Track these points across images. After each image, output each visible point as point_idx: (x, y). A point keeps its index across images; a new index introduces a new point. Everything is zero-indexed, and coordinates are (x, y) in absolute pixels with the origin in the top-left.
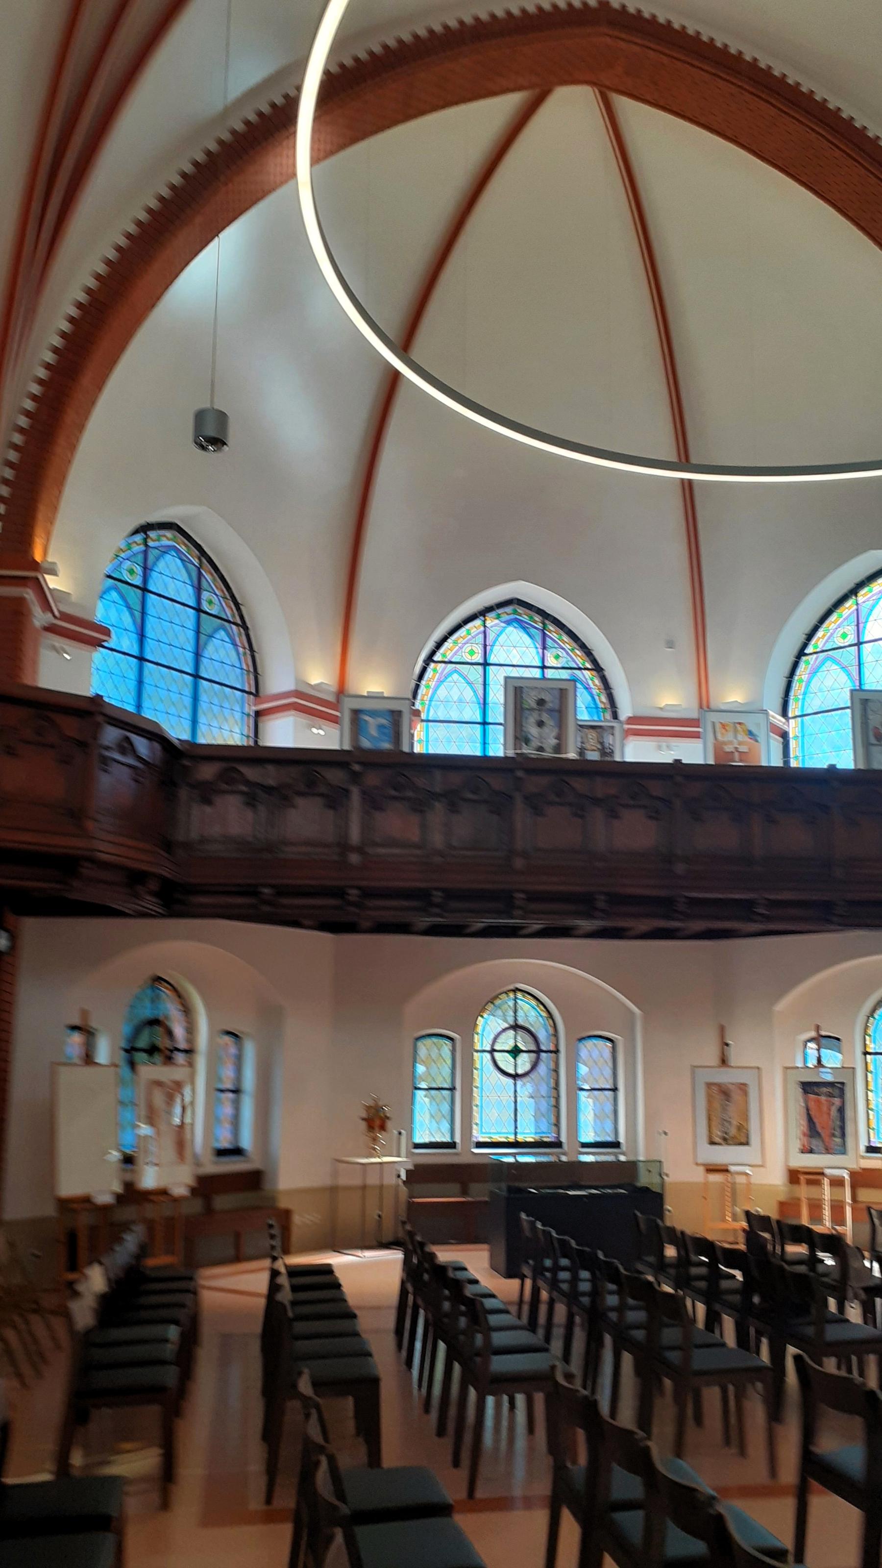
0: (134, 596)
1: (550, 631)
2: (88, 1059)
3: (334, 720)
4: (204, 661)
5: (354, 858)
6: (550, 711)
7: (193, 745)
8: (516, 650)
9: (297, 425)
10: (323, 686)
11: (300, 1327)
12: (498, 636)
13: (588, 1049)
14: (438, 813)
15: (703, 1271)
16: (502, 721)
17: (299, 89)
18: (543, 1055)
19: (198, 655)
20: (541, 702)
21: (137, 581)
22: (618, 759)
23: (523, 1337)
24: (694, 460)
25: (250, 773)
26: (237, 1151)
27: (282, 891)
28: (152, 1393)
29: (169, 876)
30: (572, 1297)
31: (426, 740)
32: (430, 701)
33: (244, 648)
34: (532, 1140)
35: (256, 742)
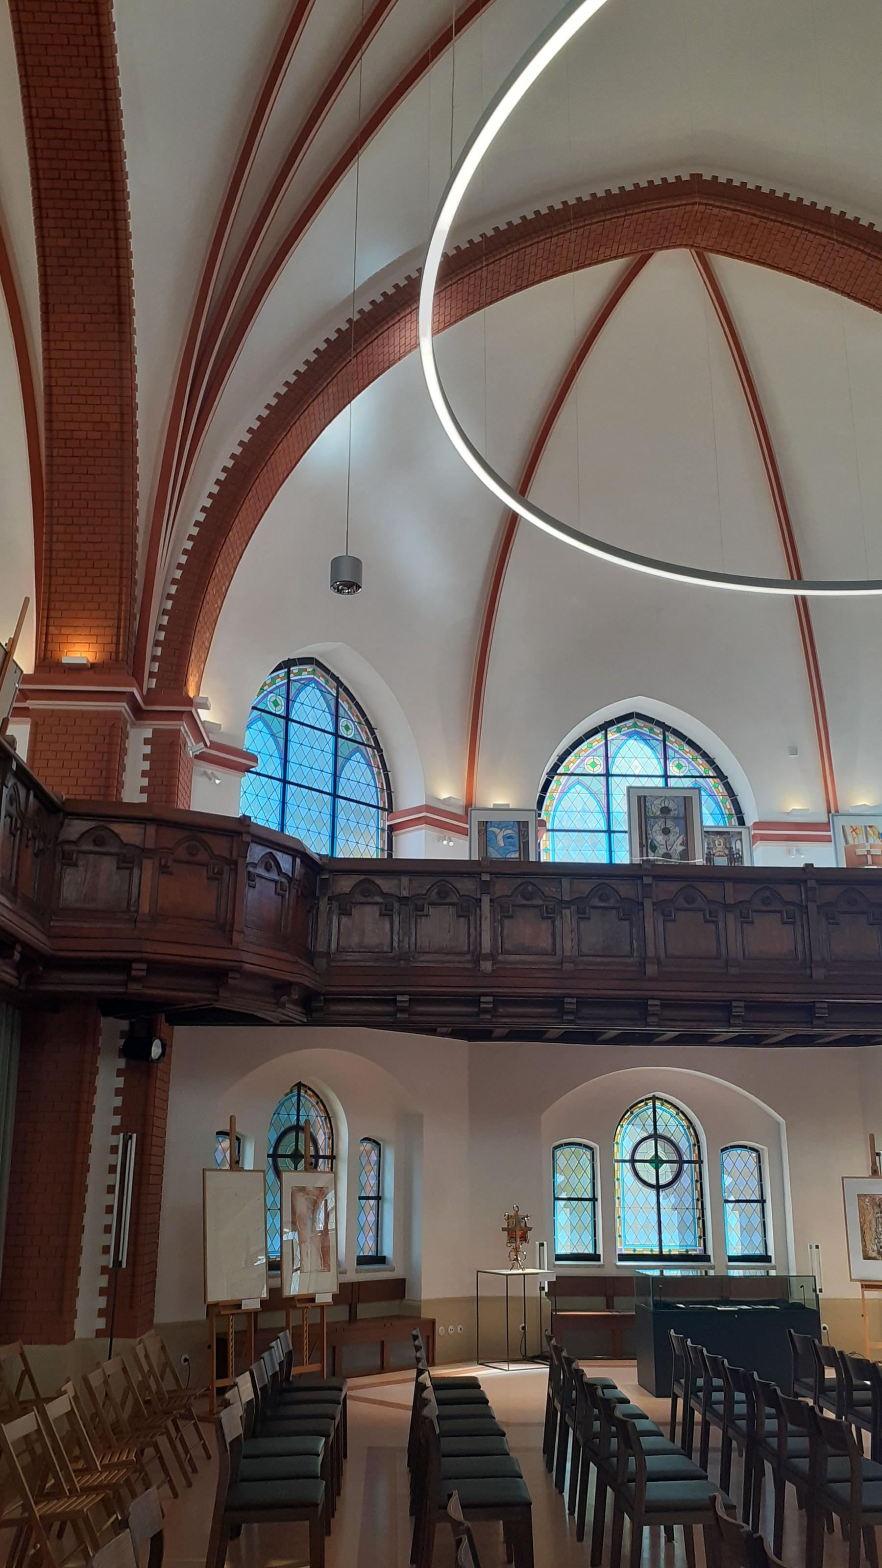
0: (278, 725)
1: (672, 743)
2: (236, 1164)
3: (464, 832)
4: (342, 782)
5: (487, 966)
6: (676, 818)
7: (332, 859)
8: (638, 760)
9: (426, 568)
10: (452, 801)
11: (448, 1444)
12: (620, 748)
13: (733, 1159)
14: (567, 919)
15: (868, 1395)
16: (626, 829)
17: (420, 271)
18: (686, 1165)
19: (336, 776)
20: (665, 810)
21: (281, 711)
22: (747, 863)
23: (676, 1463)
24: (806, 578)
25: (385, 885)
26: (379, 1260)
27: (416, 999)
28: (300, 1508)
29: (308, 984)
30: (728, 1420)
31: (553, 850)
32: (555, 811)
33: (378, 768)
34: (677, 1253)
35: (390, 855)
